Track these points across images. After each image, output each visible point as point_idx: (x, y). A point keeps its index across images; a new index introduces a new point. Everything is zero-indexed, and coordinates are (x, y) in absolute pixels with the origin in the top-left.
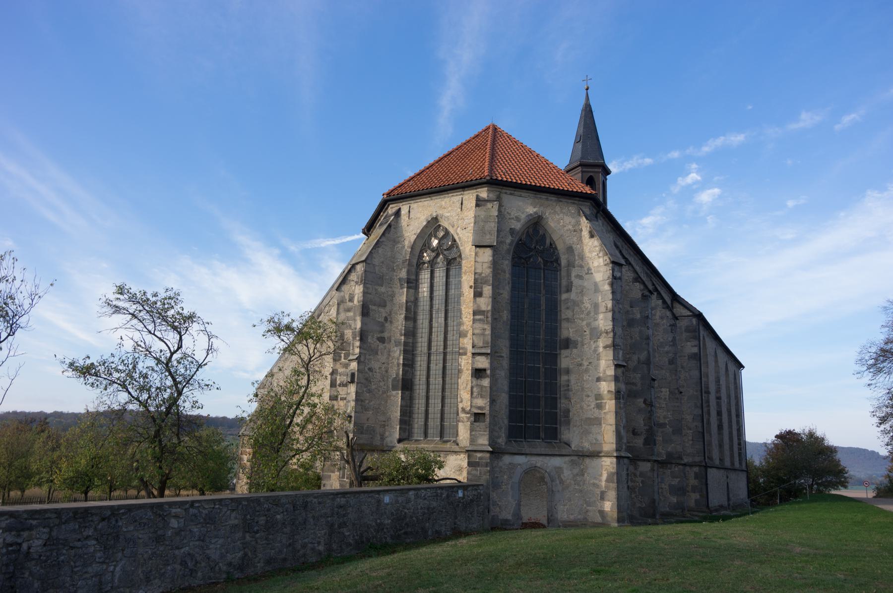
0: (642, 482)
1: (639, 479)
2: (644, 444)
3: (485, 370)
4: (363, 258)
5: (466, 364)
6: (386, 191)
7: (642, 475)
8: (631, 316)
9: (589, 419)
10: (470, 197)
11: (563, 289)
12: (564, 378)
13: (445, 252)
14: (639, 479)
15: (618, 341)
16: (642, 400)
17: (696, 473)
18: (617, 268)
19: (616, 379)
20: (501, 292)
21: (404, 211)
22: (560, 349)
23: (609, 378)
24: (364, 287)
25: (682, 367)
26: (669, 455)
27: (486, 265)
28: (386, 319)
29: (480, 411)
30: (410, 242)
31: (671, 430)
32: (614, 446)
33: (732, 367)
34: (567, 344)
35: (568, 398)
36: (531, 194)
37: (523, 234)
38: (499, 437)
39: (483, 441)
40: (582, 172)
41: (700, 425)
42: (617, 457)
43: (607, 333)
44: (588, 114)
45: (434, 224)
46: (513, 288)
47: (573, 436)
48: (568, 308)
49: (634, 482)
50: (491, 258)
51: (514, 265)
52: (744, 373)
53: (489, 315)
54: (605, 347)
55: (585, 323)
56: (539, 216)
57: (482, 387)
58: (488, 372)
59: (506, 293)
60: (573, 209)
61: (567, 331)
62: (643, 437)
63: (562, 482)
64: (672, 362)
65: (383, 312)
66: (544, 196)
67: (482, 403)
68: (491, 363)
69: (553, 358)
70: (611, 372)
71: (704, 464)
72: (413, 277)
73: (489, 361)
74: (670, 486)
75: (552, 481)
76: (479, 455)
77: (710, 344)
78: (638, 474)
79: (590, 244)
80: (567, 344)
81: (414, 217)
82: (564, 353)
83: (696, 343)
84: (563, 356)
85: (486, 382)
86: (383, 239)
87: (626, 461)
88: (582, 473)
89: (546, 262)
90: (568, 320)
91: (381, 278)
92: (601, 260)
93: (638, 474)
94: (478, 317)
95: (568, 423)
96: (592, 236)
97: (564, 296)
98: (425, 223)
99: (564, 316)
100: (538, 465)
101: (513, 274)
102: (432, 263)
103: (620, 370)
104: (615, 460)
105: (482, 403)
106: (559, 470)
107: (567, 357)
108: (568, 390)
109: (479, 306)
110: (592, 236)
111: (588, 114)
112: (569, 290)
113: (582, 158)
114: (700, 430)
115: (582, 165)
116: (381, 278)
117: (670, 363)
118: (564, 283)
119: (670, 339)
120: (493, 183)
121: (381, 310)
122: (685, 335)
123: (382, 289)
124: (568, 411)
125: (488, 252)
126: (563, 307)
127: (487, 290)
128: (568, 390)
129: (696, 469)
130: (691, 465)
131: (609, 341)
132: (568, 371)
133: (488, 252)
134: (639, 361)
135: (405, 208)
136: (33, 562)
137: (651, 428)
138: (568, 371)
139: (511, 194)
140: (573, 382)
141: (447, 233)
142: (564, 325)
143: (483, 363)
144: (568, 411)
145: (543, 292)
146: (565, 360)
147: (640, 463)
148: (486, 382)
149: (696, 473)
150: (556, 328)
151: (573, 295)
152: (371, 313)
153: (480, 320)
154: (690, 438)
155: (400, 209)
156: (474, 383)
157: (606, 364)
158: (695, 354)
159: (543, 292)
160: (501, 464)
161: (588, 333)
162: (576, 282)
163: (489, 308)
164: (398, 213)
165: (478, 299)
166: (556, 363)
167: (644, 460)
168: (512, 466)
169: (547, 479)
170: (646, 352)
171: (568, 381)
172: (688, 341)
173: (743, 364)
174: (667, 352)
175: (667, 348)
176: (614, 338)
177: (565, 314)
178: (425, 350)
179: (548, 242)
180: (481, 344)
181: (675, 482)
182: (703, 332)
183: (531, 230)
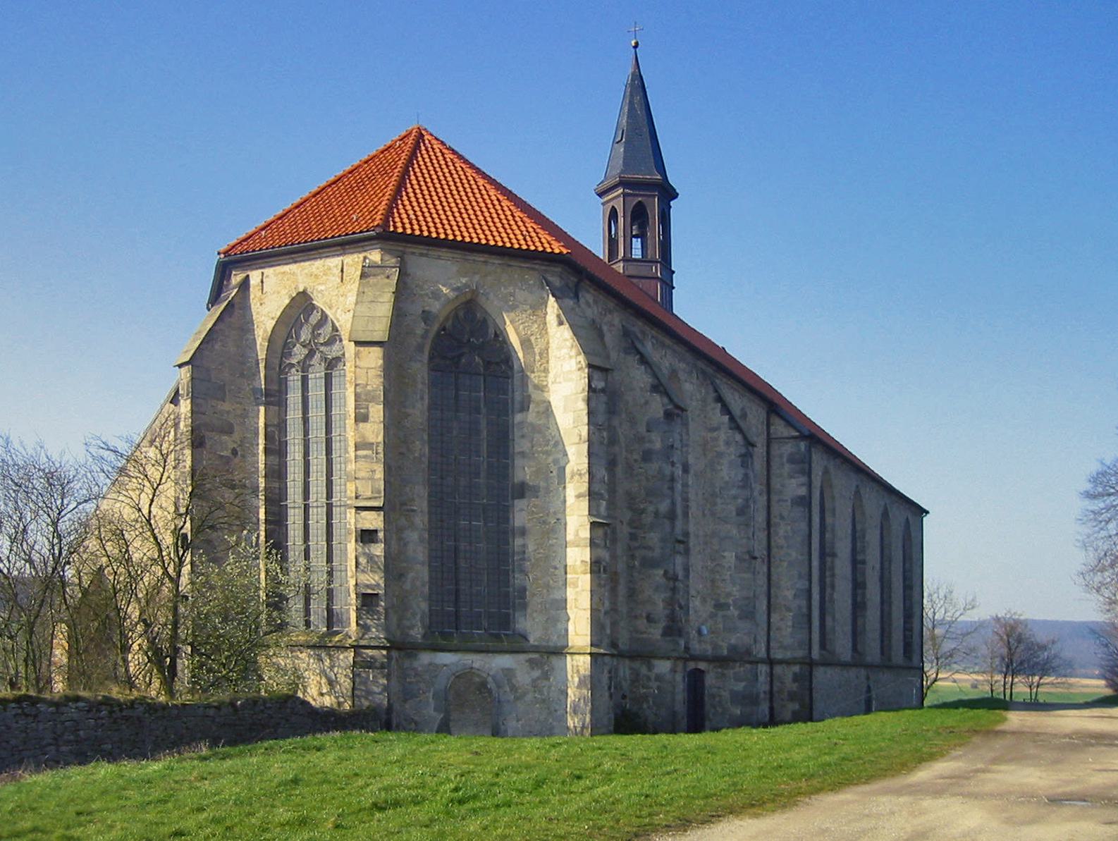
0: (658, 688)
1: (654, 684)
2: (662, 635)
3: (376, 531)
4: (187, 358)
5: (350, 521)
6: (224, 247)
7: (659, 678)
8: (647, 445)
9: (557, 600)
10: (353, 261)
11: (517, 406)
12: (518, 542)
13: (322, 348)
14: (654, 684)
15: (596, 488)
16: (662, 572)
17: (795, 674)
18: (597, 375)
19: (593, 544)
20: (410, 411)
21: (255, 276)
22: (513, 498)
23: (583, 543)
24: (192, 402)
25: (782, 518)
26: (733, 648)
27: (372, 373)
28: (234, 452)
29: (370, 591)
30: (265, 331)
31: (736, 613)
32: (588, 639)
33: (898, 516)
34: (522, 491)
35: (524, 572)
36: (458, 255)
37: (447, 319)
38: (412, 627)
39: (377, 634)
40: (625, 195)
41: (804, 603)
42: (591, 654)
43: (580, 475)
44: (638, 86)
45: (302, 305)
46: (432, 406)
47: (531, 626)
48: (523, 436)
49: (647, 687)
50: (381, 362)
51: (433, 368)
52: (926, 520)
53: (381, 449)
54: (579, 496)
55: (550, 459)
56: (473, 292)
57: (371, 558)
58: (381, 535)
59: (418, 411)
60: (532, 279)
61: (524, 472)
62: (662, 624)
63: (514, 688)
64: (741, 512)
65: (229, 442)
66: (480, 258)
67: (374, 579)
68: (386, 521)
69: (502, 514)
70: (586, 534)
71: (807, 661)
72: (276, 387)
73: (382, 518)
74: (732, 691)
75: (499, 687)
76: (370, 652)
77: (843, 483)
78: (653, 677)
79: (558, 335)
80: (522, 491)
81: (271, 292)
82: (519, 504)
83: (803, 479)
84: (516, 509)
85: (378, 550)
86: (221, 326)
87: (607, 659)
88: (546, 676)
89: (488, 364)
90: (523, 454)
91: (222, 388)
92: (573, 362)
93: (653, 677)
94: (360, 453)
95: (524, 606)
96: (561, 323)
97: (518, 417)
98: (287, 301)
99: (517, 449)
100: (476, 665)
101: (433, 384)
102: (305, 367)
103: (600, 532)
104: (588, 658)
105: (374, 579)
106: (509, 673)
107: (522, 510)
108: (523, 559)
109: (363, 437)
110: (561, 323)
111: (638, 86)
112: (524, 408)
113: (622, 172)
114: (805, 610)
115: (622, 183)
116: (222, 388)
117: (738, 514)
118: (518, 397)
119: (740, 477)
120: (386, 237)
121: (225, 438)
122: (787, 468)
123: (226, 406)
124: (524, 589)
125: (377, 352)
126: (517, 433)
127: (377, 412)
128: (523, 559)
129: (796, 668)
130: (787, 662)
131: (584, 488)
132: (523, 532)
133: (377, 352)
134: (656, 514)
135: (255, 276)
136: (571, 750)
137: (673, 611)
138: (523, 532)
139: (421, 255)
140: (531, 548)
141: (324, 317)
142: (518, 462)
143: (374, 521)
144: (523, 590)
145: (484, 410)
146: (521, 514)
147: (656, 662)
148: (378, 550)
149: (795, 674)
150: (506, 467)
151: (531, 416)
152: (208, 443)
153: (365, 457)
154: (790, 623)
155: (248, 276)
156: (360, 550)
157: (577, 520)
158: (802, 498)
159: (484, 410)
160: (416, 664)
161: (555, 473)
162: (535, 395)
163: (380, 439)
164: (245, 284)
165: (361, 425)
166: (507, 520)
167: (662, 658)
168: (434, 668)
169: (491, 685)
170: (668, 501)
171: (524, 546)
172: (791, 477)
173: (926, 508)
174: (735, 497)
175: (734, 492)
176: (590, 483)
177: (521, 445)
178: (299, 500)
179: (491, 331)
180: (369, 494)
181: (740, 687)
182: (819, 461)
183: (461, 314)
